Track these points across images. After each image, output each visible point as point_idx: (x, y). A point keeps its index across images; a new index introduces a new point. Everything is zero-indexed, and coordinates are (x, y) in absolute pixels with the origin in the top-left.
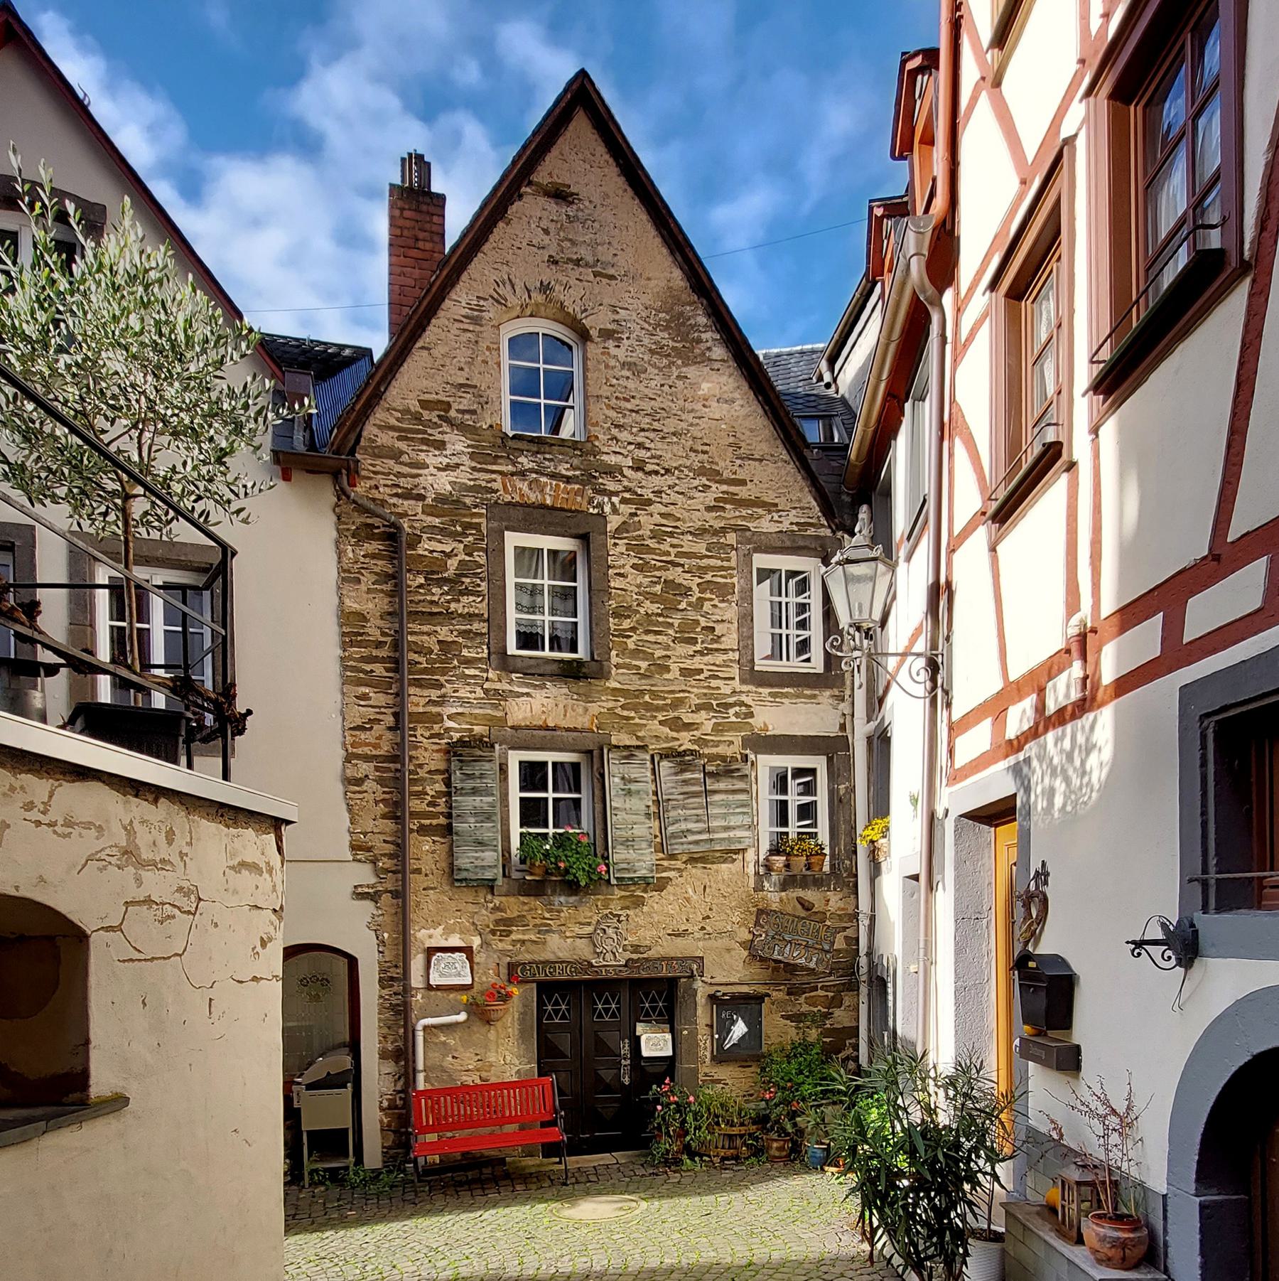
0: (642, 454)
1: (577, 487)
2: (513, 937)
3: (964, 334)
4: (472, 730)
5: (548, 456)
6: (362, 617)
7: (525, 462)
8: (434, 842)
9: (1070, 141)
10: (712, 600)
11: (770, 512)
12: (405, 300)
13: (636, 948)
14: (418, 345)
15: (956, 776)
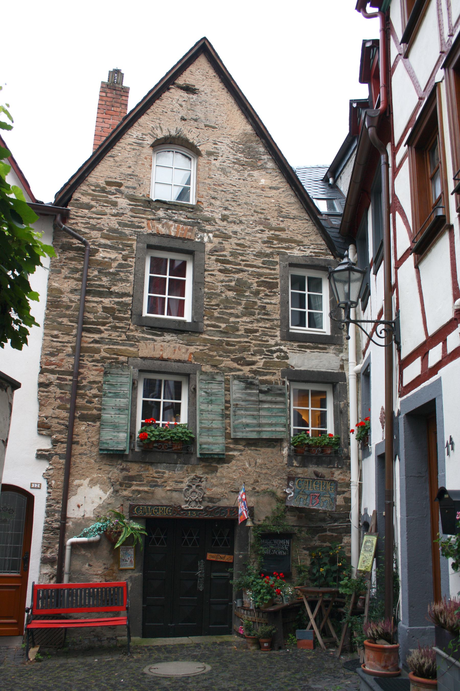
0: (226, 213)
1: (189, 227)
2: (134, 488)
3: (397, 164)
4: (118, 359)
5: (174, 211)
6: (60, 292)
8: (89, 425)
9: (437, 85)
10: (265, 291)
11: (299, 245)
12: (103, 134)
13: (211, 500)
15: (404, 390)
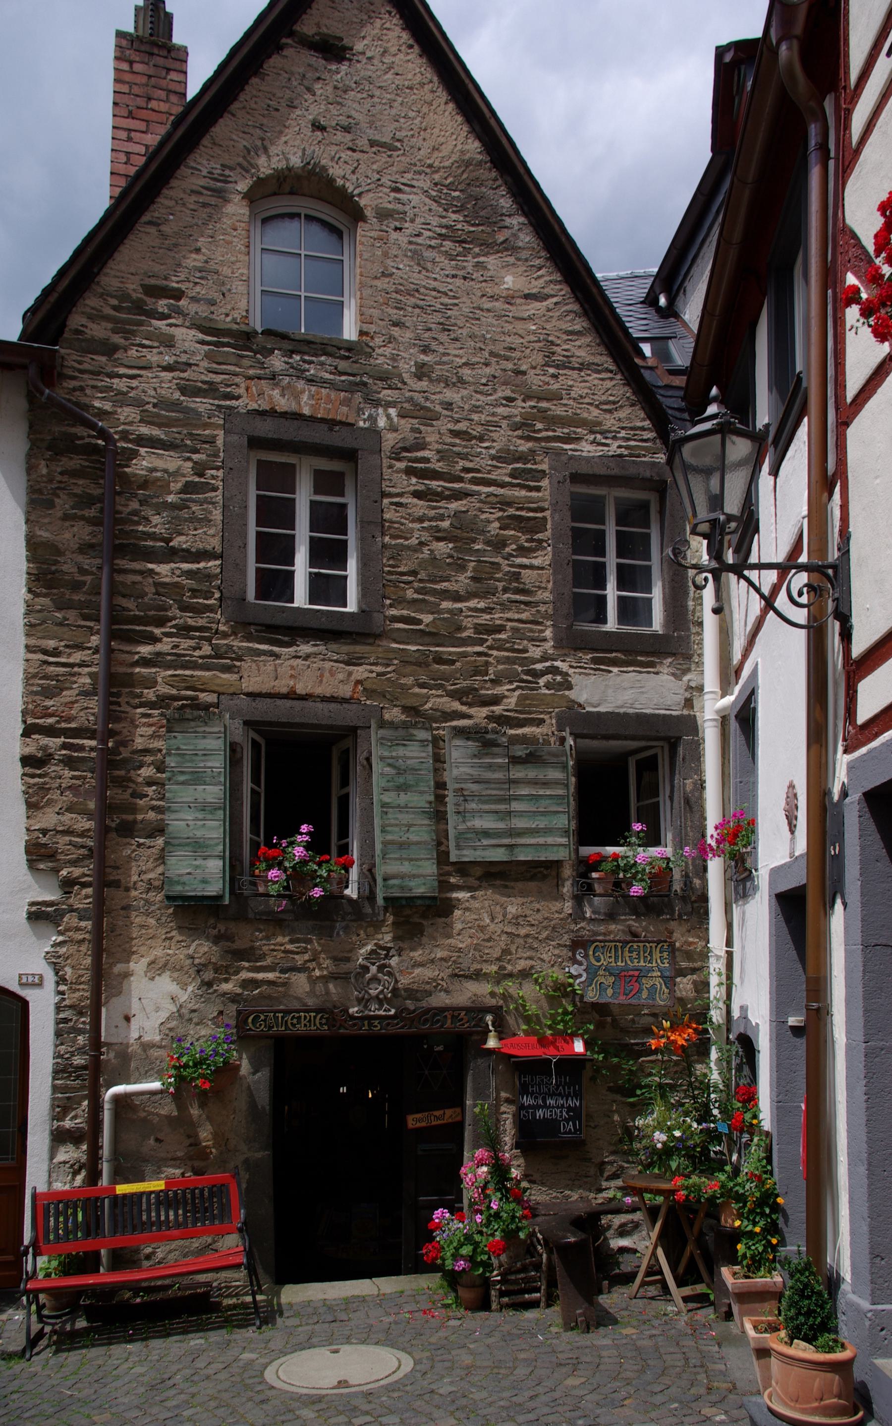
7: (277, 362)
14: (145, 218)
